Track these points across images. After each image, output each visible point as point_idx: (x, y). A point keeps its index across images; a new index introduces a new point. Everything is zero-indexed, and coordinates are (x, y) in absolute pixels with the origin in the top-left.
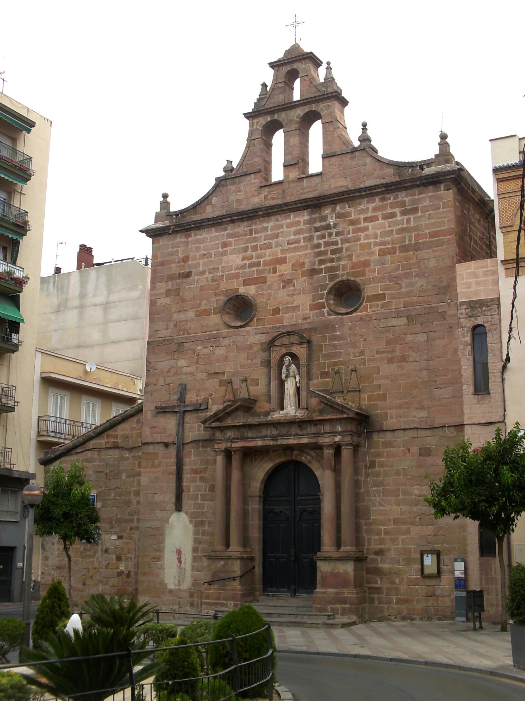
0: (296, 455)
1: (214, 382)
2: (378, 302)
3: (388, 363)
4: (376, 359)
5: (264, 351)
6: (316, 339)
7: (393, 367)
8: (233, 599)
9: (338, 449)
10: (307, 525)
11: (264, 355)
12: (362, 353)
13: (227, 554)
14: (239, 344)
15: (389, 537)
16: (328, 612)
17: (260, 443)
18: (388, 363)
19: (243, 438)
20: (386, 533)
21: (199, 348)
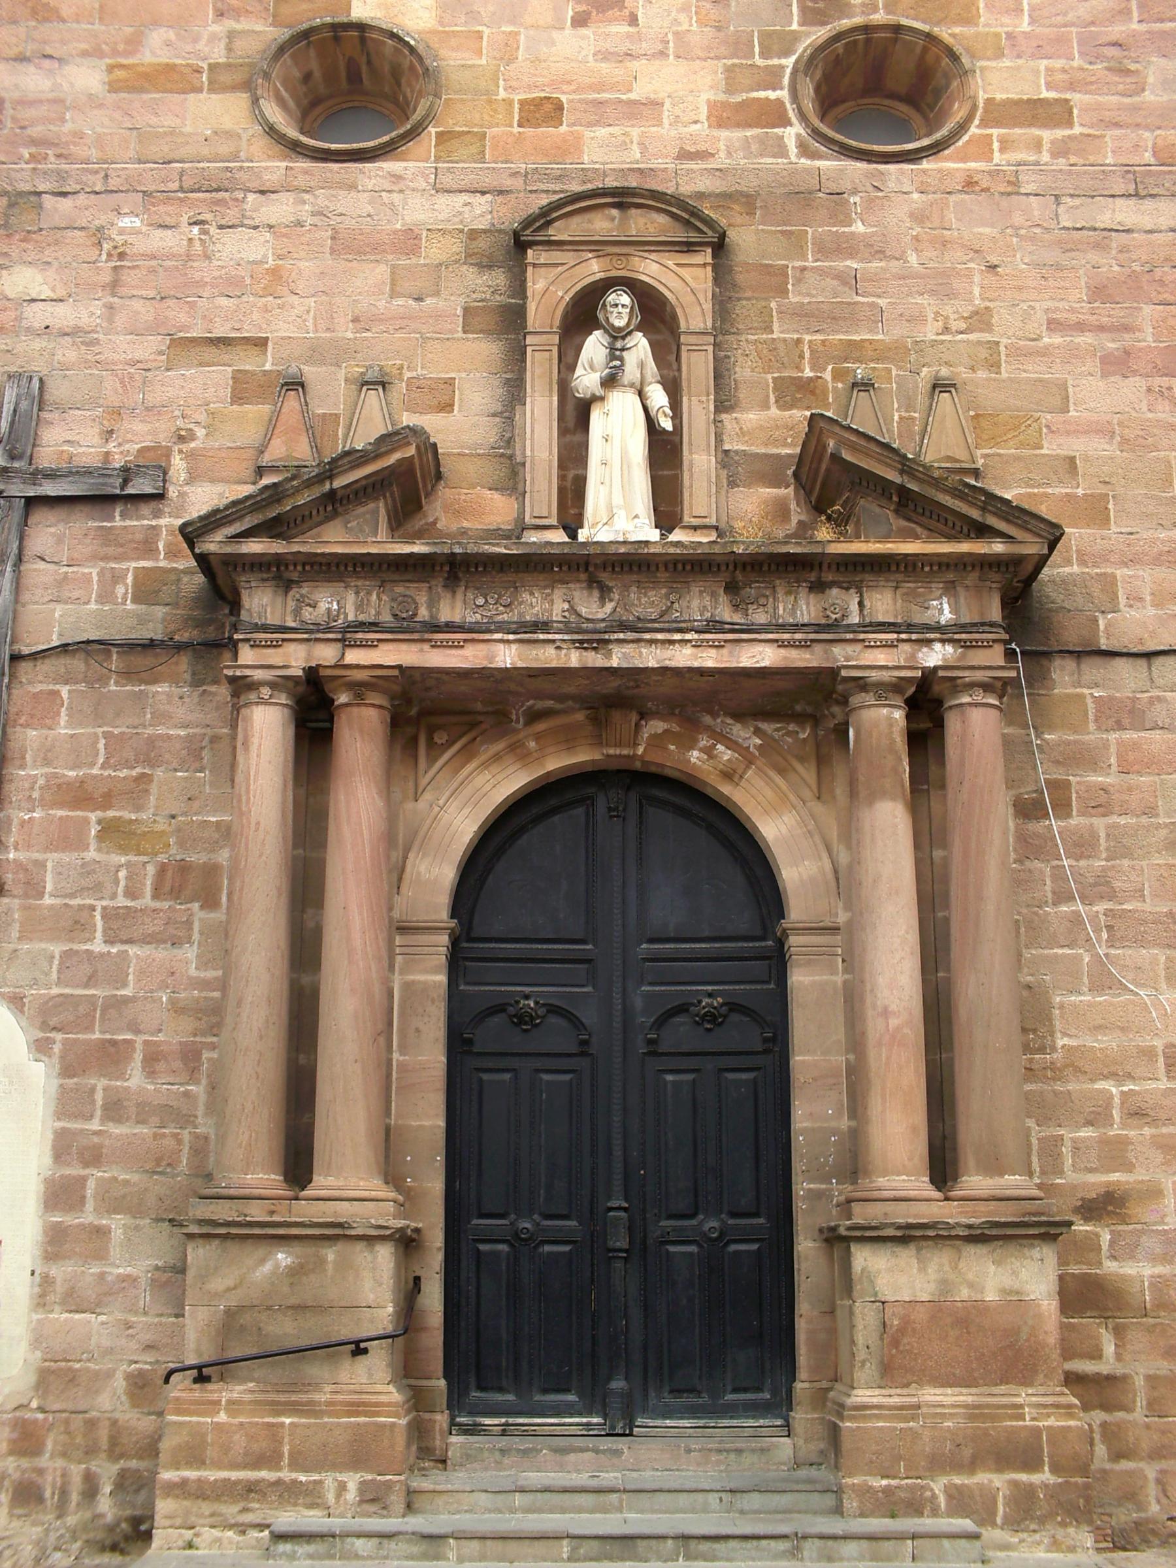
0: (657, 741)
1: (208, 382)
2: (1037, 132)
3: (1105, 375)
4: (1045, 352)
5: (485, 264)
6: (746, 238)
7: (1129, 393)
8: (356, 1462)
9: (926, 703)
10: (690, 1077)
11: (489, 285)
12: (980, 319)
13: (305, 1211)
14: (349, 222)
15: (1147, 1131)
16: (935, 1513)
17: (506, 655)
18: (1105, 375)
19: (407, 628)
20: (1137, 1113)
21: (126, 222)
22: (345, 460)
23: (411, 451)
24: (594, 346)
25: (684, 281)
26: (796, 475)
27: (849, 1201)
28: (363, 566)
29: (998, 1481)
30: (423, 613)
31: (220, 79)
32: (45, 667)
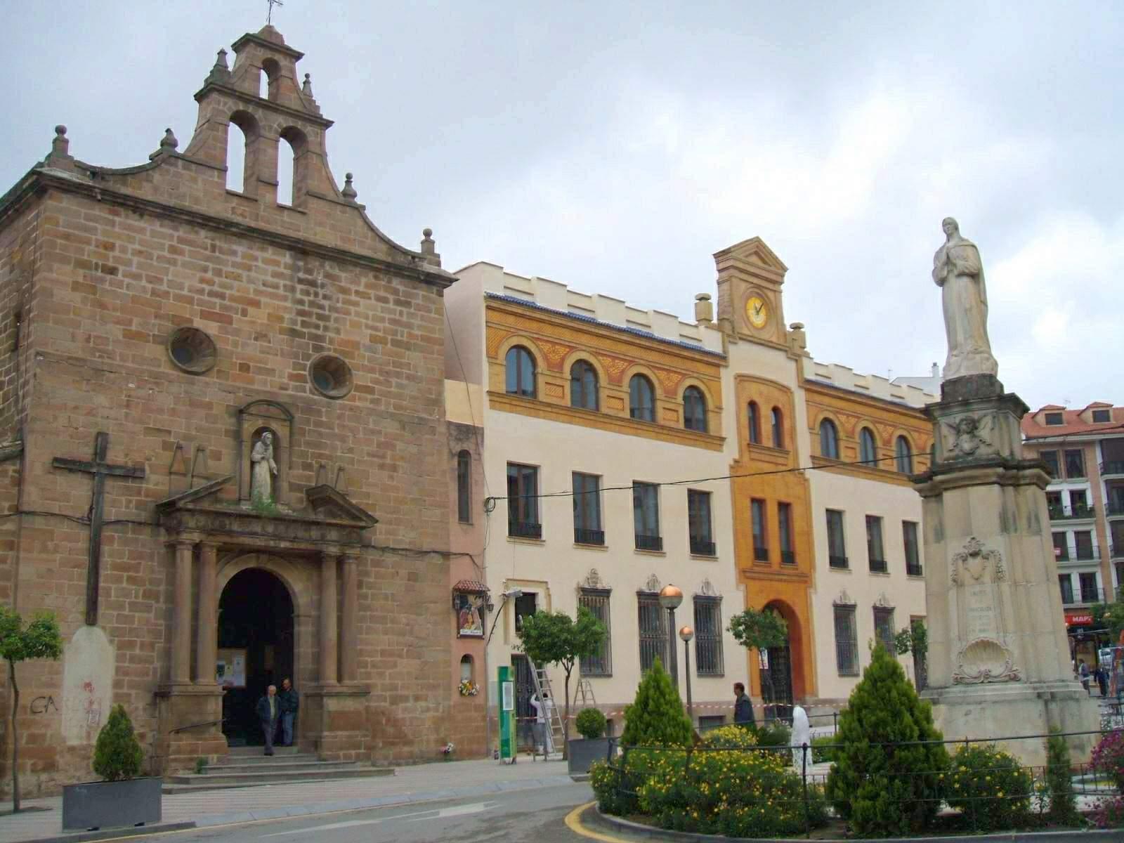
1: (156, 440)
5: (231, 416)
8: (216, 752)
20: (374, 666)
25: (282, 430)
29: (353, 752)
31: (158, 340)
32: (111, 527)
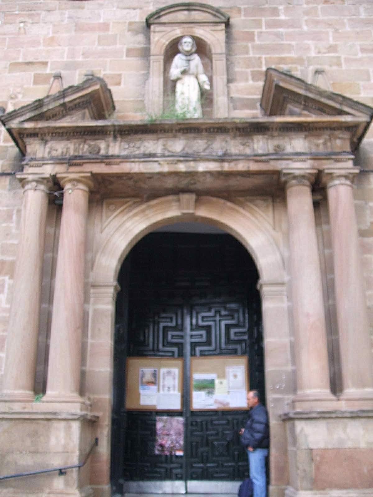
4: (360, 60)
9: (318, 187)
22: (70, 90)
23: (97, 87)
24: (179, 61)
25: (214, 37)
26: (261, 105)
27: (293, 402)
28: (77, 132)
30: (103, 152)
